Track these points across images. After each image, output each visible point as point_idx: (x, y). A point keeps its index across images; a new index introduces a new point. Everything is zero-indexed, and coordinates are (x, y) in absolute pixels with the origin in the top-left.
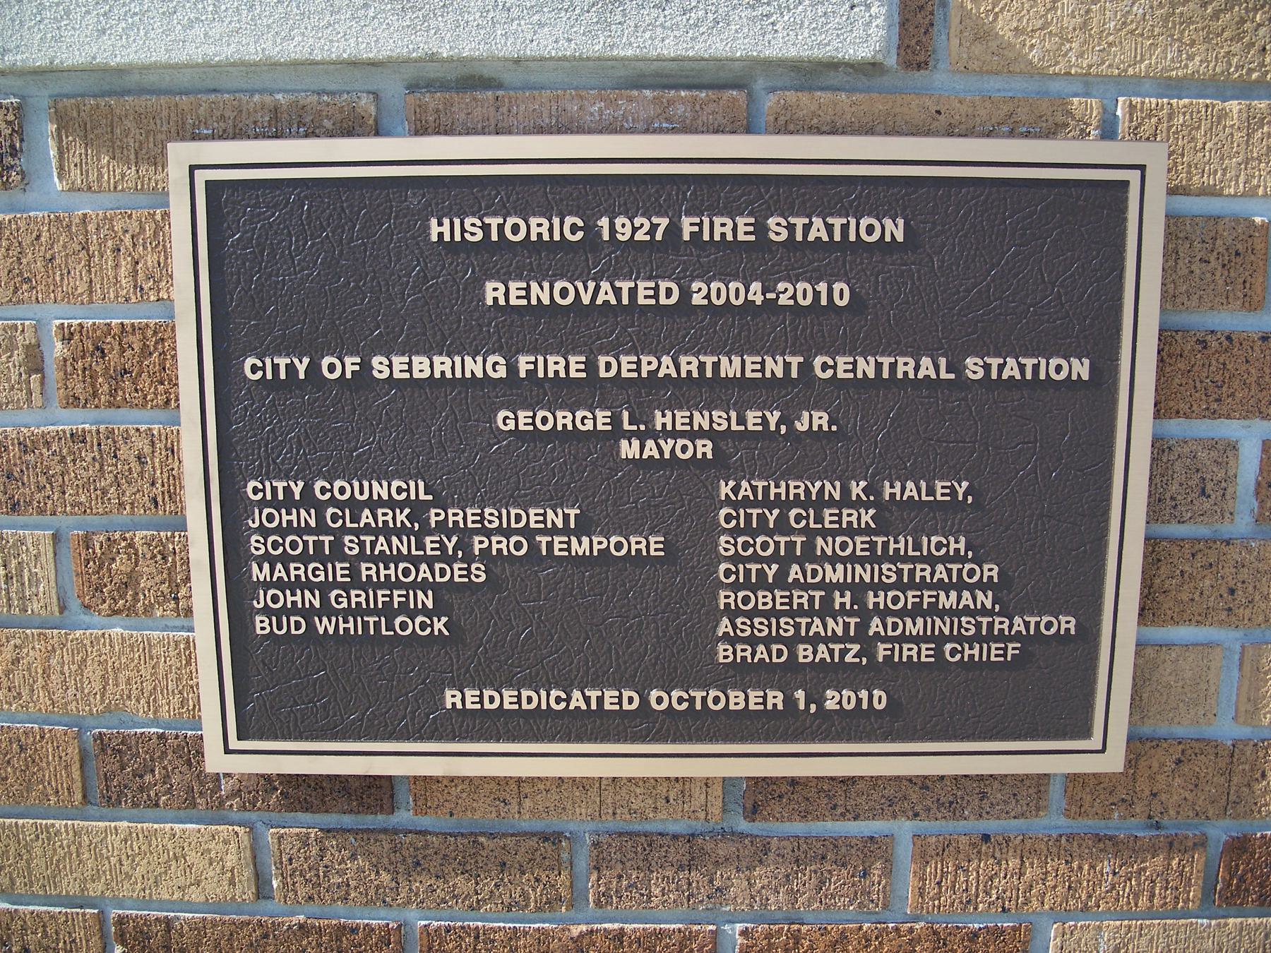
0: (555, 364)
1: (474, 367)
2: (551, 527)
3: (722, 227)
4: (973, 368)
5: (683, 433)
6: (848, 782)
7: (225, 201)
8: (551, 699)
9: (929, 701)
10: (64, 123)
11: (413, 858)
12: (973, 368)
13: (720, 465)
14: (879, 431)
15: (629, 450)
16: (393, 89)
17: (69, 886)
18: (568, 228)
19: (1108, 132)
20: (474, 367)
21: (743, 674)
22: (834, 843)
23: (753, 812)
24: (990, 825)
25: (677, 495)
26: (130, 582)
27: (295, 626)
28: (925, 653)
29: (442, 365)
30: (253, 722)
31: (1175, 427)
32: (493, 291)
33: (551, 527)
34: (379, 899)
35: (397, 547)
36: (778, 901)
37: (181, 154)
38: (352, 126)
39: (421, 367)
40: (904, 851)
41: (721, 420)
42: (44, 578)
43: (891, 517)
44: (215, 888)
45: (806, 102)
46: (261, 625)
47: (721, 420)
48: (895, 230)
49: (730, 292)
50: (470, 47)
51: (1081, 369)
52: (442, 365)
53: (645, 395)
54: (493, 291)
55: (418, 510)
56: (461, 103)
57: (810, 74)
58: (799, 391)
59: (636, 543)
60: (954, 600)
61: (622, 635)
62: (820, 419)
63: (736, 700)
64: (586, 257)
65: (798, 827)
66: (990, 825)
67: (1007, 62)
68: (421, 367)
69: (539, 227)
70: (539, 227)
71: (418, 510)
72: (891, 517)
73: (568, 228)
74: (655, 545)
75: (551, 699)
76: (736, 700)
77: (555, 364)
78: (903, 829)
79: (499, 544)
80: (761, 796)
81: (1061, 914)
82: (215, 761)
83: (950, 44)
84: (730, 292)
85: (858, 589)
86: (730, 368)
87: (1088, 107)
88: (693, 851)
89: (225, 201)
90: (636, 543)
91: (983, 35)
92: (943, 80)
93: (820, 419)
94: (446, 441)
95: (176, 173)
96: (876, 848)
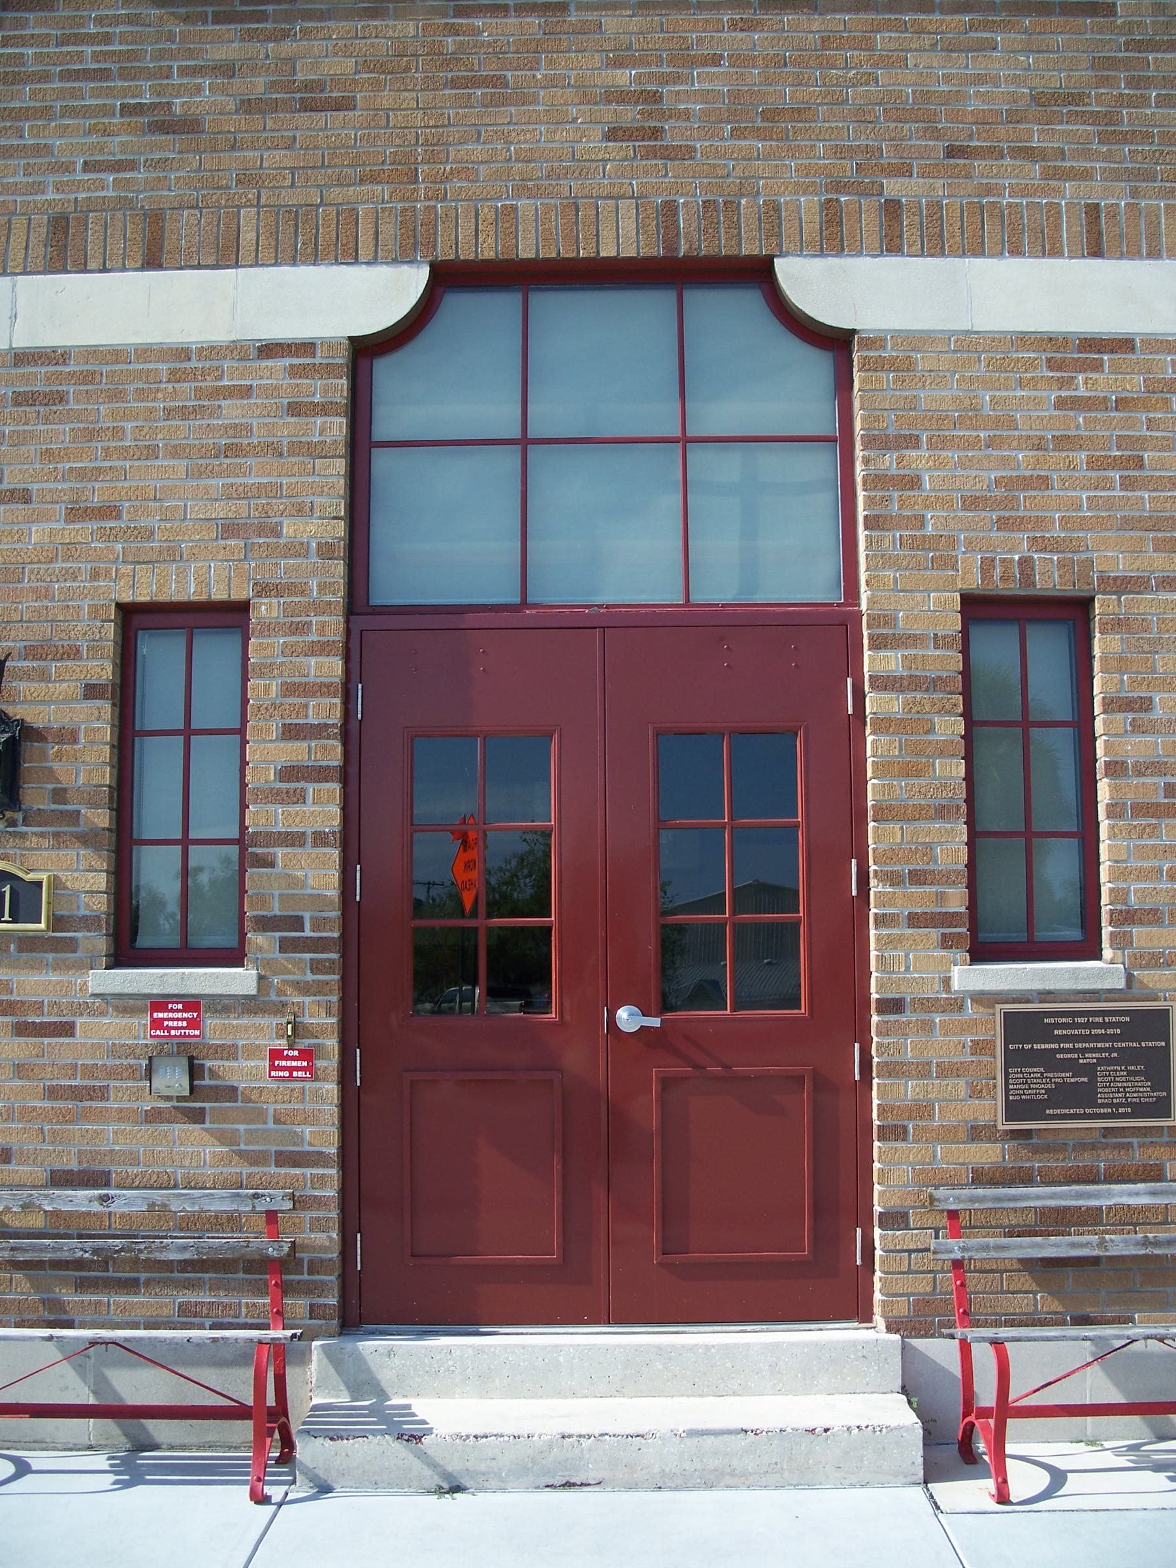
0: (1067, 1045)
1: (1052, 1046)
2: (1068, 1077)
3: (1097, 1019)
4: (1143, 1044)
5: (1091, 1058)
6: (1123, 1128)
7: (1007, 1016)
8: (1066, 1111)
9: (1140, 1110)
10: (972, 1000)
11: (1036, 1150)
12: (1143, 1044)
13: (1098, 1064)
14: (1127, 1057)
15: (1081, 1061)
16: (1035, 994)
17: (961, 1160)
18: (1069, 1020)
19: (1165, 1000)
20: (1052, 1046)
21: (1103, 1105)
22: (1122, 1143)
23: (1105, 1137)
24: (1153, 1140)
25: (1090, 1070)
26: (981, 1091)
27: (1018, 1098)
28: (1137, 1100)
29: (1047, 1046)
30: (1009, 1117)
31: (1165, 1131)
32: (1056, 1032)
33: (1068, 1077)
34: (1029, 1160)
35: (1038, 1082)
36: (1111, 1157)
37: (998, 1007)
38: (1028, 1001)
39: (1043, 1046)
40: (1136, 1145)
41: (1098, 1055)
42: (963, 1092)
43: (1130, 1073)
44: (994, 1159)
45: (1110, 996)
46: (1011, 1098)
47: (1098, 1055)
48: (1128, 1019)
49: (1098, 1031)
50: (1052, 987)
51: (1163, 1044)
52: (1047, 1046)
53: (1084, 1051)
54: (1056, 1032)
55: (1042, 1074)
56: (1049, 997)
57: (1110, 991)
58: (1110, 1050)
59: (1083, 1079)
60: (1142, 1091)
61: (1079, 1097)
62: (1116, 1055)
63: (1102, 1111)
64: (1087, 1025)
65: (1114, 1140)
66: (1153, 1140)
67: (1146, 987)
68: (1043, 1046)
69: (1064, 1020)
70: (1064, 1020)
71: (1042, 1074)
72: (1130, 1073)
73: (1069, 1020)
74: (1086, 1080)
75: (1066, 1111)
76: (1102, 1111)
77: (1067, 1045)
78: (1135, 1141)
79: (1058, 1080)
80: (1107, 1132)
81: (1170, 1160)
82: (1000, 1127)
83: (1135, 984)
84: (1098, 1031)
85: (1124, 1088)
86: (1099, 1045)
87: (1161, 995)
88: (1093, 1147)
89: (1007, 1016)
90: (1083, 1079)
91: (1141, 982)
92: (1135, 991)
93: (1116, 1055)
94: (1048, 1061)
95: (998, 1010)
96: (1130, 1144)
